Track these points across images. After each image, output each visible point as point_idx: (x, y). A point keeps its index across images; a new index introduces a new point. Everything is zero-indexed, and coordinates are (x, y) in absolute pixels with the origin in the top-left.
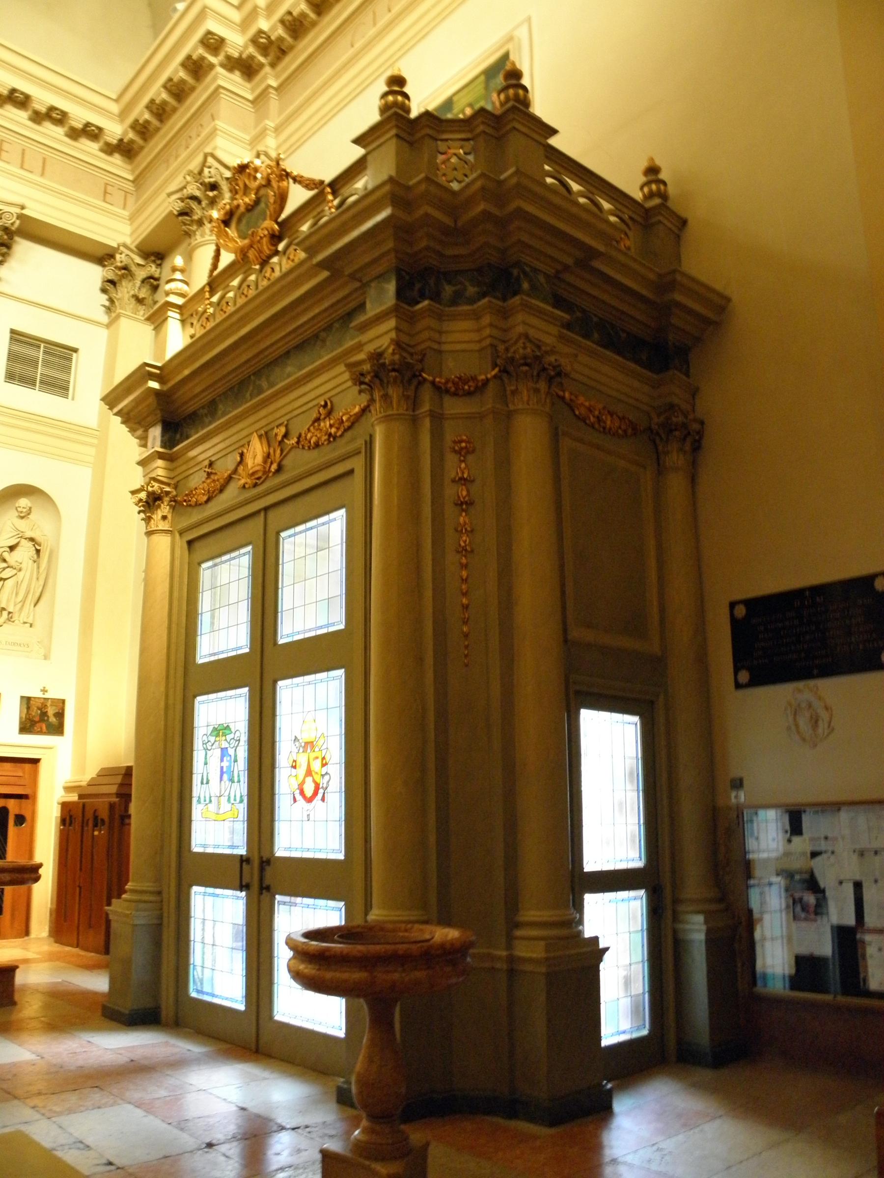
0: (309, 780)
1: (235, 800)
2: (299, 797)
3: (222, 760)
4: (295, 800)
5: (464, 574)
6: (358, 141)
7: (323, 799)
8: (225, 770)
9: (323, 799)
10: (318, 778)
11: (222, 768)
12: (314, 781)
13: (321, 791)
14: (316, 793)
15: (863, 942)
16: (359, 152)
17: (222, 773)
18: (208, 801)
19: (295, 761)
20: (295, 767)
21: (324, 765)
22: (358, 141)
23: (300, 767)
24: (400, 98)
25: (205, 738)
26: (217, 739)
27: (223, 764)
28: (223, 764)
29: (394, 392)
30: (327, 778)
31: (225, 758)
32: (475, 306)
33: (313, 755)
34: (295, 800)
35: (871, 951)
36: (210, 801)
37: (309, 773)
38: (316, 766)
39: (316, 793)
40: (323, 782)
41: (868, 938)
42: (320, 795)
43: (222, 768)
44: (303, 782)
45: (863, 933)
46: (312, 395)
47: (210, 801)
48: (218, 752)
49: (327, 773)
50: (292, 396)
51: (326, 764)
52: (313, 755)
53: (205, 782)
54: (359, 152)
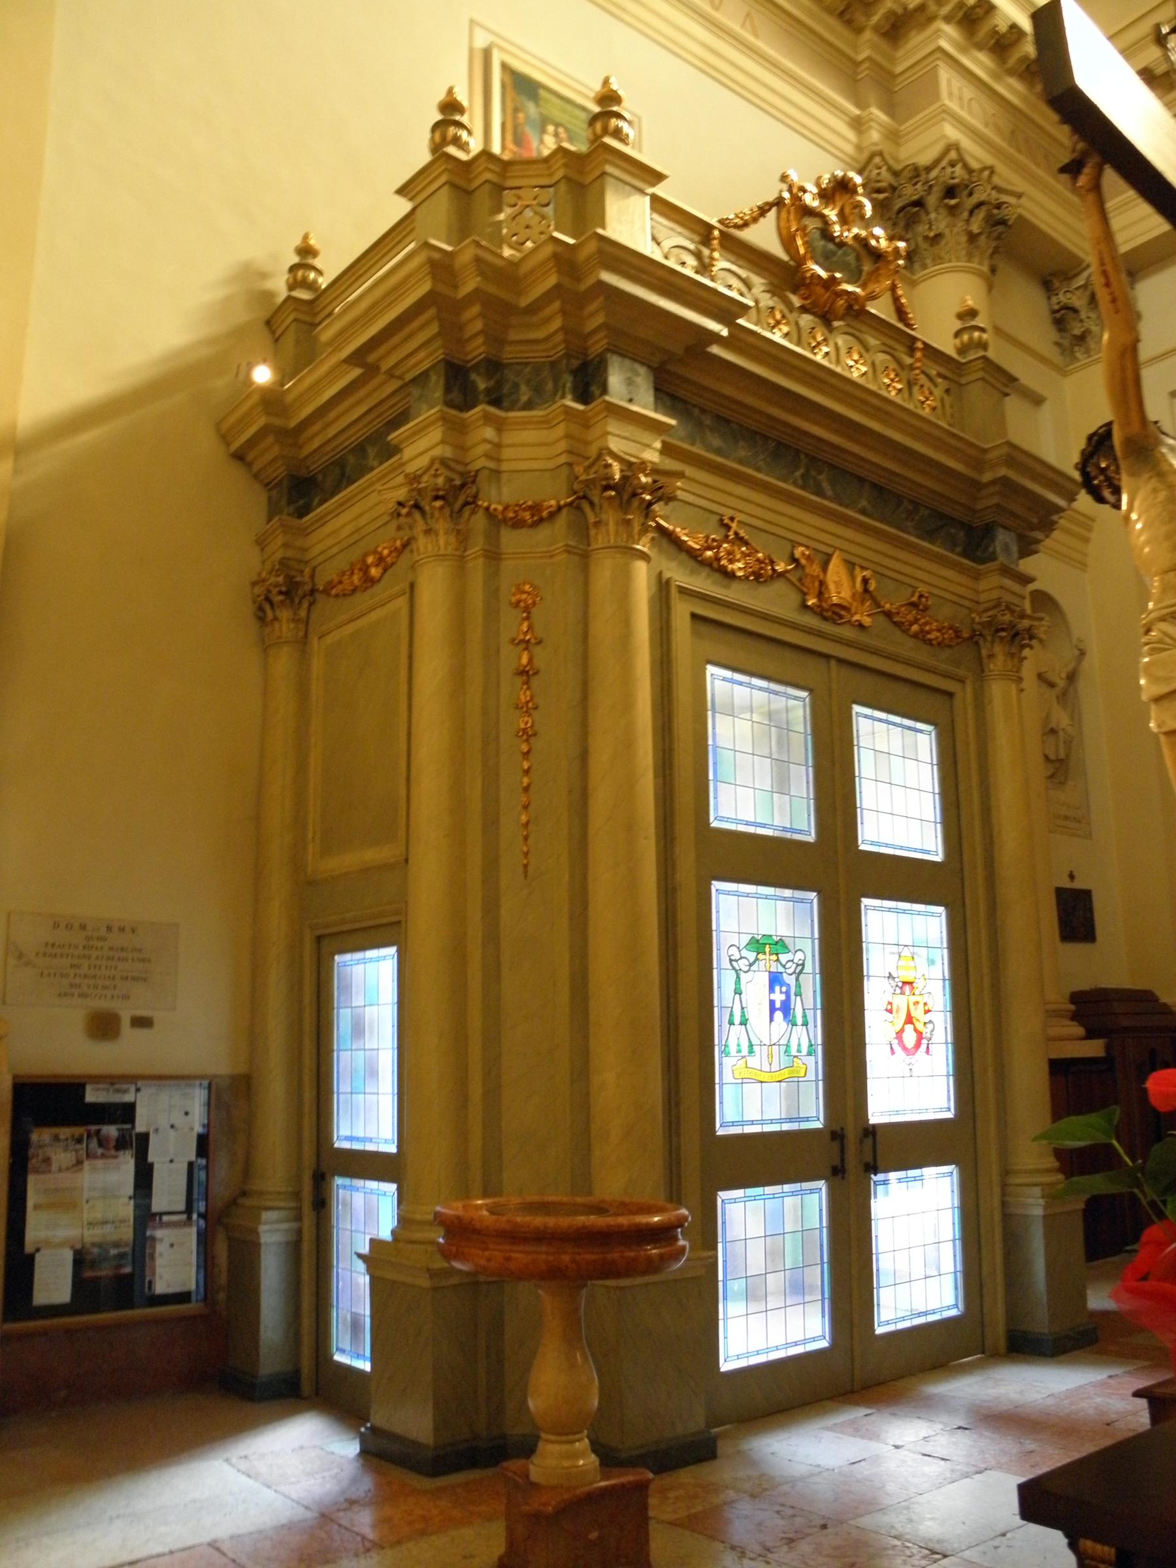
0: (909, 1027)
1: (799, 1051)
2: (897, 1048)
3: (772, 990)
4: (893, 1052)
5: (526, 780)
6: (402, 191)
7: (928, 1051)
8: (778, 1005)
9: (928, 1051)
10: (920, 1027)
11: (772, 1003)
12: (916, 1030)
13: (924, 1042)
14: (918, 1045)
15: (153, 1239)
16: (403, 206)
17: (773, 1010)
18: (745, 1052)
19: (890, 1003)
20: (890, 1011)
21: (927, 1012)
22: (402, 191)
23: (897, 1011)
24: (976, 334)
25: (734, 951)
26: (761, 956)
27: (773, 997)
28: (773, 997)
29: (442, 525)
30: (930, 1026)
31: (777, 988)
32: (981, 567)
33: (913, 999)
34: (893, 1052)
35: (160, 1248)
36: (751, 1051)
37: (909, 1020)
38: (917, 1013)
39: (918, 1045)
40: (926, 1031)
41: (159, 1233)
42: (923, 1048)
43: (772, 1003)
44: (902, 1030)
45: (154, 1228)
46: (919, 574)
47: (751, 1051)
48: (764, 978)
49: (930, 1022)
50: (924, 563)
51: (929, 1011)
52: (913, 999)
53: (737, 1020)
54: (403, 206)
